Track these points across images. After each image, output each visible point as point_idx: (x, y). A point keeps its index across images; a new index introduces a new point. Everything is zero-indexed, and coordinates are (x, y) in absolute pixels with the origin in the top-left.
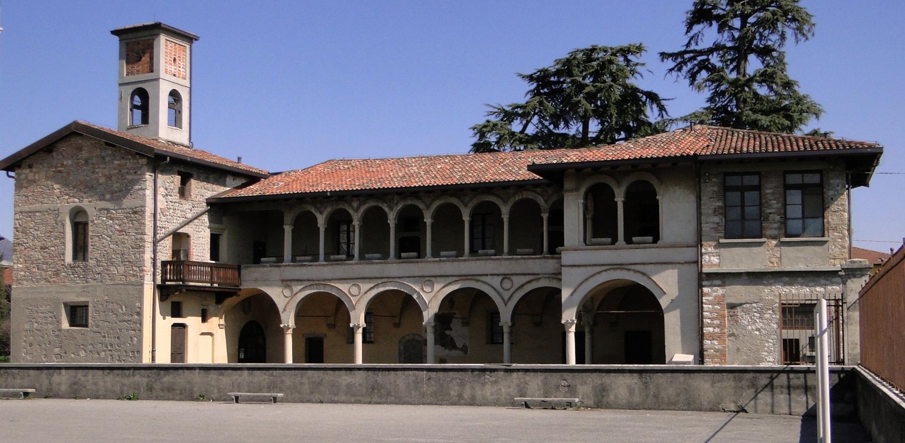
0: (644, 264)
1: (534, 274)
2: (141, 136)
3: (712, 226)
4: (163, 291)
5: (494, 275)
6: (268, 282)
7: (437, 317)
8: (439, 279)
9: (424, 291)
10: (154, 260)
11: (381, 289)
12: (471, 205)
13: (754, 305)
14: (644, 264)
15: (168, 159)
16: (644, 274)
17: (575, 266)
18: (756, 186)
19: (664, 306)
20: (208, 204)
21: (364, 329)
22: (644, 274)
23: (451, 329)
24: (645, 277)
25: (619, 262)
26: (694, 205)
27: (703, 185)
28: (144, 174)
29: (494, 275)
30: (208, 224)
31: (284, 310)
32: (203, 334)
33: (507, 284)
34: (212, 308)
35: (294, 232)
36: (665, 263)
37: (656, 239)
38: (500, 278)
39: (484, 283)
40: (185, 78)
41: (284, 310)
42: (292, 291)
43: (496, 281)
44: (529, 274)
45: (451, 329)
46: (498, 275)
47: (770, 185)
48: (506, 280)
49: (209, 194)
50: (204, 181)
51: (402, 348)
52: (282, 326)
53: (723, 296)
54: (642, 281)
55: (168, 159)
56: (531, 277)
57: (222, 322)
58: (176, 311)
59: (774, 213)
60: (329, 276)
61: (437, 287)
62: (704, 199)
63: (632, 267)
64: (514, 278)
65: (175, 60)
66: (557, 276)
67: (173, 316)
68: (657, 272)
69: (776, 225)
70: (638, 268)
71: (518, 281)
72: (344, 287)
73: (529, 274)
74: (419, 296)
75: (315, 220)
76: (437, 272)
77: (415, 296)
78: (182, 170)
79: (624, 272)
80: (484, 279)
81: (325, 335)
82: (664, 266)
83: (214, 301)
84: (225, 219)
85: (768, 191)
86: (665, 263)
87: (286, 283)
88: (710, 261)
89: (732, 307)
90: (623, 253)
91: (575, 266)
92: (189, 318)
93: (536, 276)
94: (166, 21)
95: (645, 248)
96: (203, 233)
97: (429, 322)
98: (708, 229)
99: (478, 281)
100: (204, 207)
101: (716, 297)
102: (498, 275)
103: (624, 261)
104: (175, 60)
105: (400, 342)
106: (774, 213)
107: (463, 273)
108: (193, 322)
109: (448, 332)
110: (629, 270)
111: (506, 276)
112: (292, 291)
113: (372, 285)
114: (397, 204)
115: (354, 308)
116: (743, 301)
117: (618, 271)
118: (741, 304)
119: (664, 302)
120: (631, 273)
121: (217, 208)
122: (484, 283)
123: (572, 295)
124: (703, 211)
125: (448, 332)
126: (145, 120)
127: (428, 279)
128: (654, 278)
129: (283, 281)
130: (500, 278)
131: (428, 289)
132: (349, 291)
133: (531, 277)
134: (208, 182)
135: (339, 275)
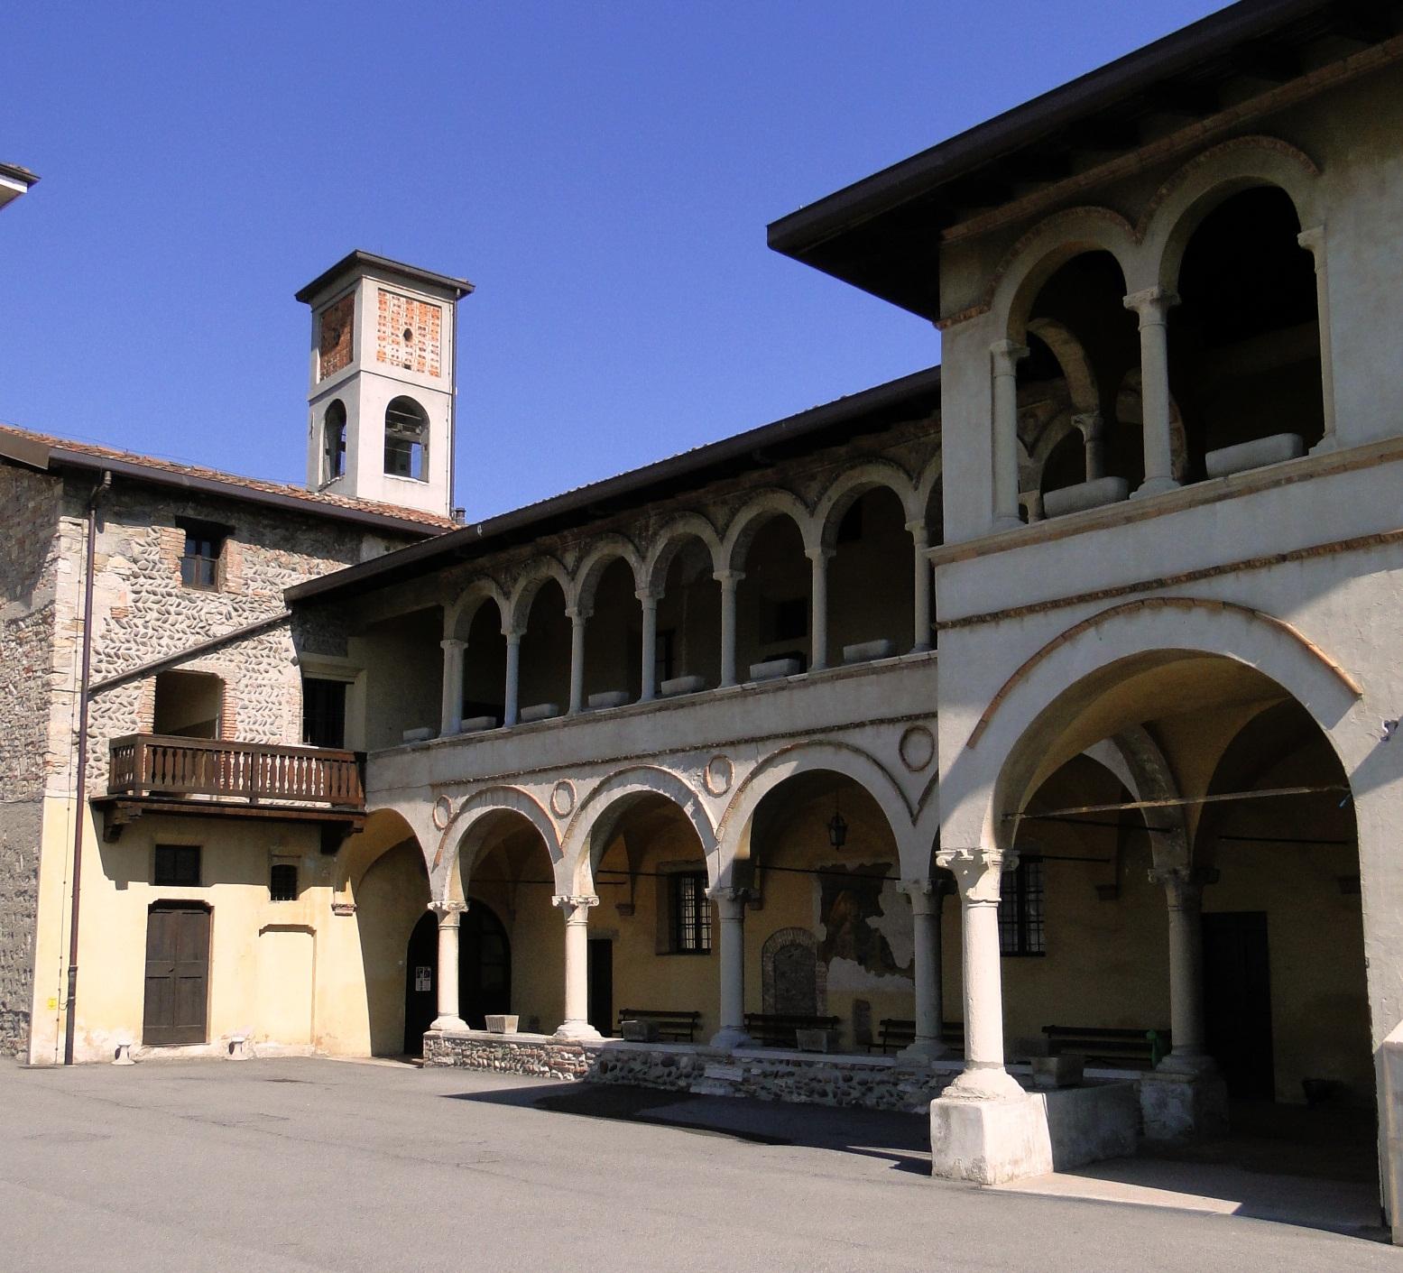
0: (1249, 565)
2: (338, 498)
4: (113, 818)
5: (881, 721)
6: (406, 791)
7: (740, 868)
8: (743, 748)
9: (709, 792)
10: (82, 737)
11: (617, 793)
12: (825, 507)
14: (1249, 565)
15: (108, 477)
16: (1251, 613)
17: (980, 619)
19: (1350, 765)
20: (290, 603)
21: (592, 912)
22: (1251, 613)
23: (880, 914)
24: (1259, 632)
25: (1147, 574)
28: (56, 523)
29: (881, 721)
30: (293, 653)
31: (436, 865)
32: (261, 932)
34: (309, 863)
35: (468, 656)
36: (1349, 545)
37: (1309, 427)
39: (857, 751)
40: (435, 374)
41: (436, 865)
42: (448, 810)
43: (884, 742)
45: (880, 914)
46: (892, 721)
49: (297, 579)
50: (275, 546)
51: (770, 968)
52: (430, 906)
54: (1242, 648)
55: (108, 477)
57: (347, 897)
58: (177, 865)
60: (514, 765)
61: (740, 771)
63: (1200, 589)
65: (408, 335)
67: (159, 881)
68: (1313, 592)
70: (1227, 587)
72: (539, 792)
74: (699, 808)
76: (740, 729)
77: (689, 809)
78: (190, 513)
79: (1170, 616)
80: (855, 738)
81: (617, 931)
82: (1347, 559)
83: (318, 845)
84: (354, 644)
86: (1349, 545)
87: (438, 791)
90: (1169, 531)
91: (980, 619)
92: (217, 886)
94: (370, 248)
95: (1252, 489)
96: (273, 674)
97: (719, 888)
99: (839, 746)
100: (279, 609)
102: (892, 721)
103: (1169, 568)
104: (408, 335)
105: (764, 950)
107: (802, 724)
108: (236, 905)
109: (873, 922)
110: (1190, 603)
112: (448, 810)
113: (595, 782)
114: (652, 540)
115: (561, 855)
117: (1146, 617)
119: (1352, 740)
120: (1199, 616)
121: (306, 608)
122: (857, 751)
123: (972, 742)
125: (873, 922)
126: (336, 467)
127: (713, 754)
128: (1302, 625)
129: (433, 786)
130: (893, 734)
131: (717, 783)
132: (553, 808)
134: (293, 549)
135: (533, 761)
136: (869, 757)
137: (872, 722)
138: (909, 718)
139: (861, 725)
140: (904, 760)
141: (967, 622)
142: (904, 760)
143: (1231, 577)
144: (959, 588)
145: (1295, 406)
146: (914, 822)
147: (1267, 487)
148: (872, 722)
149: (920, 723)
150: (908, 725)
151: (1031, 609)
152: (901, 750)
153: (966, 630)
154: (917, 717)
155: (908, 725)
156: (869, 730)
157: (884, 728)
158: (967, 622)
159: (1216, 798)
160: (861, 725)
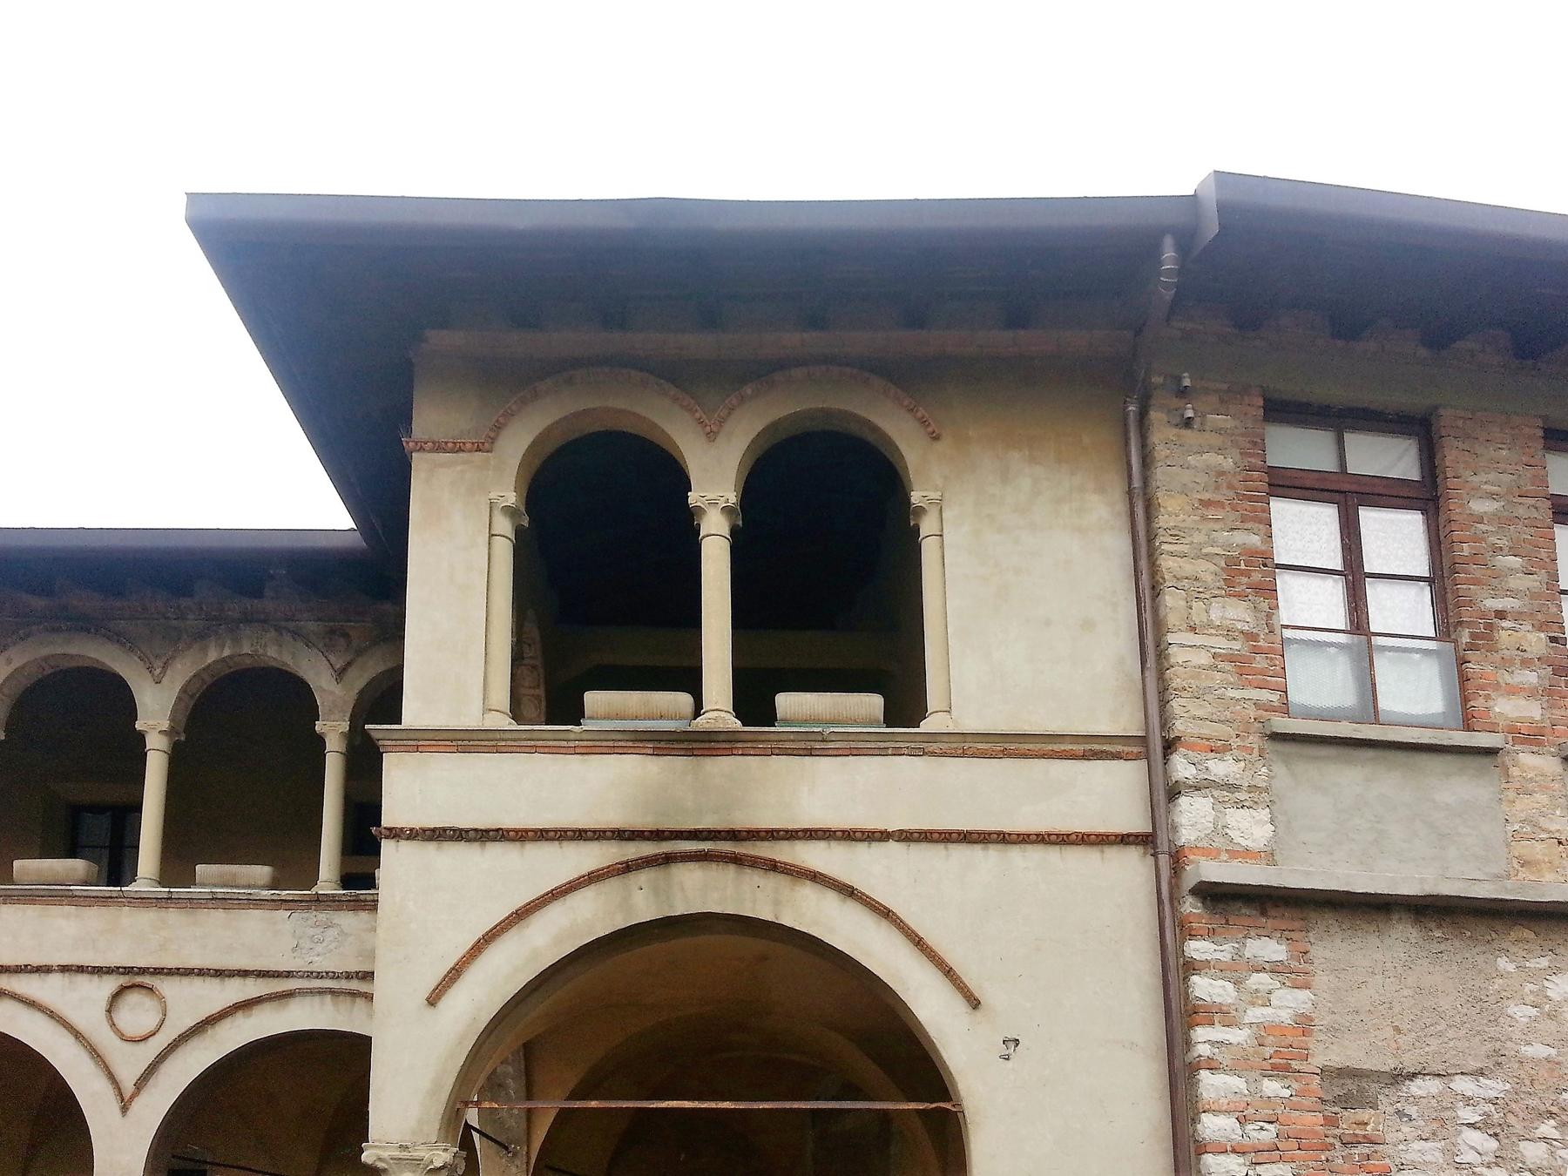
1: (277, 975)
3: (1222, 644)
5: (81, 969)
13: (1463, 1085)
18: (1147, 836)
26: (1118, 544)
27: (1162, 434)
29: (81, 969)
33: (137, 1014)
38: (111, 984)
39: (31, 1004)
44: (244, 973)
46: (98, 971)
47: (1486, 480)
48: (133, 998)
53: (1304, 1024)
56: (253, 988)
59: (1518, 616)
62: (1172, 511)
64: (166, 986)
66: (357, 984)
69: (1530, 678)
71: (191, 1001)
73: (244, 973)
75: (129, 709)
79: (725, 876)
85: (1480, 506)
88: (1220, 830)
89: (1350, 1087)
93: (280, 984)
95: (1025, 756)
98: (1204, 659)
101: (1263, 1032)
102: (98, 971)
106: (1518, 616)
111: (134, 979)
116: (1409, 1063)
118: (1398, 1077)
122: (31, 1004)
124: (1167, 563)
130: (111, 984)
133: (253, 988)
136: (52, 1015)
137: (65, 969)
138: (128, 971)
139: (44, 970)
140: (113, 1025)
141: (414, 835)
142: (113, 1025)
143: (820, 846)
144: (411, 789)
145: (888, 663)
146: (124, 1110)
147: (1037, 757)
148: (65, 969)
149: (146, 980)
150: (123, 980)
151: (542, 835)
152: (109, 1011)
153: (431, 847)
154: (143, 971)
155: (123, 980)
156: (55, 979)
157: (82, 980)
158: (414, 835)
159: (578, 1104)
160: (44, 970)
